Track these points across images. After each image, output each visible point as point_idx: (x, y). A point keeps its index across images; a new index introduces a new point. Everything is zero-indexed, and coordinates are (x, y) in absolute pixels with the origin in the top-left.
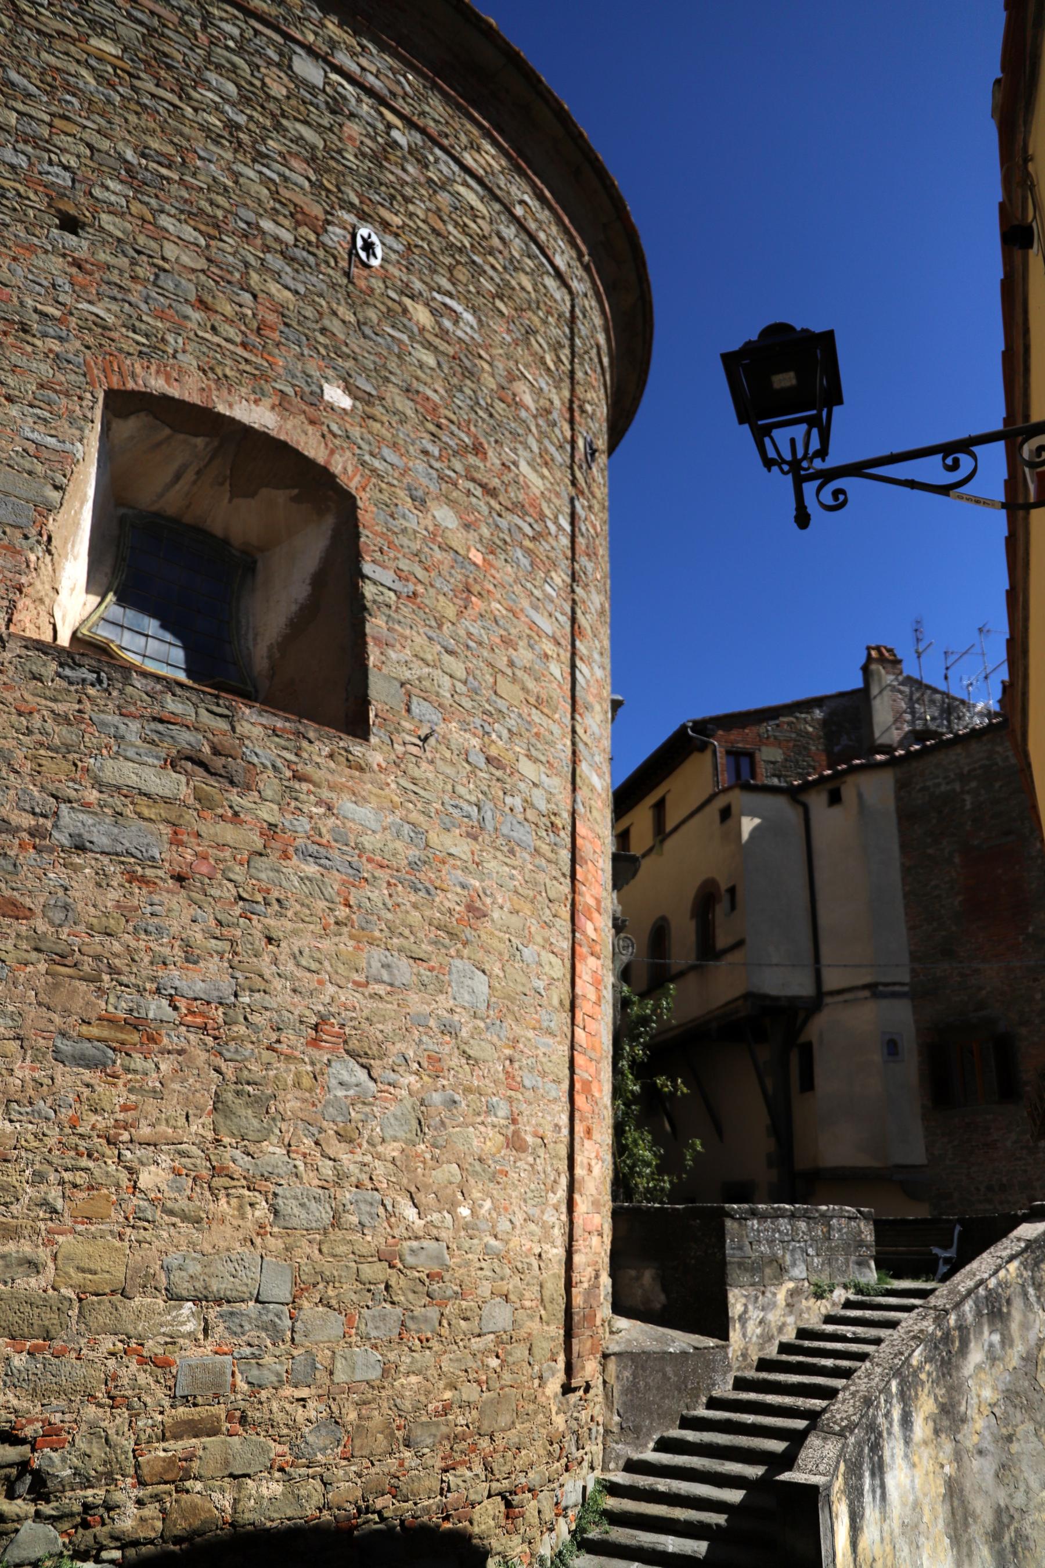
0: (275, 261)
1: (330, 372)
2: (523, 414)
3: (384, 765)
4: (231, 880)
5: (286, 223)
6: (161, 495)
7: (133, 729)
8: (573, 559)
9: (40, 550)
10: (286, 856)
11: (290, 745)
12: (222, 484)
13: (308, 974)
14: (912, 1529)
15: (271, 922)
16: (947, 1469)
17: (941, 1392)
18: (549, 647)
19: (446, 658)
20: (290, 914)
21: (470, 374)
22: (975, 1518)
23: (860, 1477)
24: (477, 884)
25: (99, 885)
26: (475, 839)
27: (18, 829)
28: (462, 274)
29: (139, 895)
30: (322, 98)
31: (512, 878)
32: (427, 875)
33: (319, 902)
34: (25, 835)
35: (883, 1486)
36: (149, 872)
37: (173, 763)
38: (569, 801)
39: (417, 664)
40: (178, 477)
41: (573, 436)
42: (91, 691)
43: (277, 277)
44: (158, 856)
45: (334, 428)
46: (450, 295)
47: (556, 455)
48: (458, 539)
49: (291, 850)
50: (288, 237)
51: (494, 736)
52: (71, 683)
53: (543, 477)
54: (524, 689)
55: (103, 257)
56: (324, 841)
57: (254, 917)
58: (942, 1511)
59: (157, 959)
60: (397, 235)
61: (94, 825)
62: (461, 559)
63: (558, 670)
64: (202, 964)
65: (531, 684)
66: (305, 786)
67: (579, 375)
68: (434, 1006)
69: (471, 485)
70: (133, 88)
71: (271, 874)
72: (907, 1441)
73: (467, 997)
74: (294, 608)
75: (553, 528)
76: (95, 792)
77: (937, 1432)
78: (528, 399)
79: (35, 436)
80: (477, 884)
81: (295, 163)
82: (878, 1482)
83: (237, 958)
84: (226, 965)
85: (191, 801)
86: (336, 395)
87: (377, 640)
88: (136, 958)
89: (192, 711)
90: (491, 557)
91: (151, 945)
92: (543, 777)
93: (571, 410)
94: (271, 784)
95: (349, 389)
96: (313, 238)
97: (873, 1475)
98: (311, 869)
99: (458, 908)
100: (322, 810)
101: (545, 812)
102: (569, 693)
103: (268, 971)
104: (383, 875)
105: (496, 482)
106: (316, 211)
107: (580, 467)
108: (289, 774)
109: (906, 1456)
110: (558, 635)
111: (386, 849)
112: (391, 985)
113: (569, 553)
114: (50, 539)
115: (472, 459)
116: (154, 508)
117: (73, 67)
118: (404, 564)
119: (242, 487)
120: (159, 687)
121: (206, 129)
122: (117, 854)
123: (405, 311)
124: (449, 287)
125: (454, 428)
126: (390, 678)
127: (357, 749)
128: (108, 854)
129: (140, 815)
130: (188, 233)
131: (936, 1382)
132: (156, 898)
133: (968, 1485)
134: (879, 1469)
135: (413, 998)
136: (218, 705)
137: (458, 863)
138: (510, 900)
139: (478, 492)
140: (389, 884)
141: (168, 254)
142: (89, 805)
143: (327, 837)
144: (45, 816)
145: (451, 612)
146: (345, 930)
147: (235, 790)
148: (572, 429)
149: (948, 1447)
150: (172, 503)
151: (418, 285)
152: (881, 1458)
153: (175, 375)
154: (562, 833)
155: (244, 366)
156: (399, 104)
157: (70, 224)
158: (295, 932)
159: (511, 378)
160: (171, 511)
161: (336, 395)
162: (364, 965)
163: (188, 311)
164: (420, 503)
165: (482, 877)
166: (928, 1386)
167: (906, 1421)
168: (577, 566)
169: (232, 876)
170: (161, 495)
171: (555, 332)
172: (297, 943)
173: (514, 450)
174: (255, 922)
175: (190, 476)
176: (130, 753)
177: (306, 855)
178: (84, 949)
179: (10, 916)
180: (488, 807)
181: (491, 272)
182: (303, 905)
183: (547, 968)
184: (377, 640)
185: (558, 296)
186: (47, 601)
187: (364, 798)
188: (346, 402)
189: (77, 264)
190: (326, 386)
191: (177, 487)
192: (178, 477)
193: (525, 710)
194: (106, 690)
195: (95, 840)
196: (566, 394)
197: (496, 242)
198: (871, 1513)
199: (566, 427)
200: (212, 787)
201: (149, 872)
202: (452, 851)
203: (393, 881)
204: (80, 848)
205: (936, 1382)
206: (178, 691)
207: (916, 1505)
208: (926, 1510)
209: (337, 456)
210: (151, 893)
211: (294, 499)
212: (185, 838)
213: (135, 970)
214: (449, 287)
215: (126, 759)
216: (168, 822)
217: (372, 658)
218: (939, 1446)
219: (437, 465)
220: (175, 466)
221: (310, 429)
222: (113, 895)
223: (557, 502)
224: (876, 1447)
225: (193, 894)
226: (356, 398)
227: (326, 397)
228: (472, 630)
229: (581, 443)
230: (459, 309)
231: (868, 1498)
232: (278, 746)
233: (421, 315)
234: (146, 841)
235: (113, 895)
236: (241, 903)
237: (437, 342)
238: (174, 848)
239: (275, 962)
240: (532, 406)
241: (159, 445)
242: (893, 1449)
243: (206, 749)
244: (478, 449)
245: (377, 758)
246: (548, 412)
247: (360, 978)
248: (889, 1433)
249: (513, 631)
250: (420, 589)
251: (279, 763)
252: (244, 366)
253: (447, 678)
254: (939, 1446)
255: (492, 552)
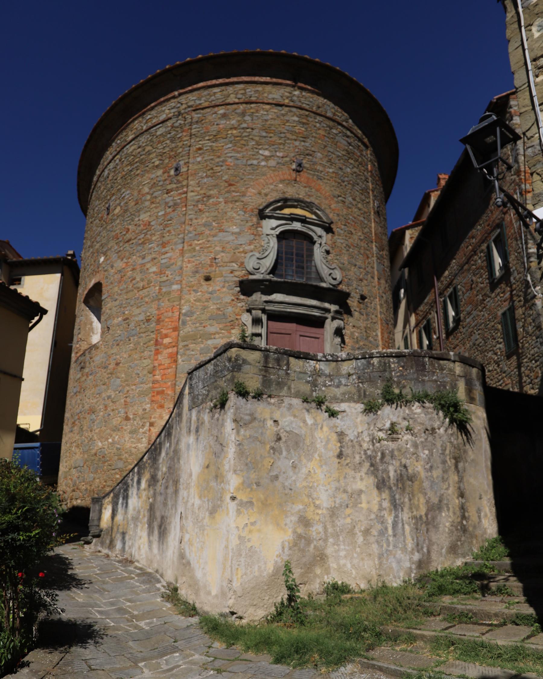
14: (136, 519)
16: (151, 500)
17: (152, 470)
22: (156, 519)
23: (118, 499)
35: (127, 503)
58: (147, 514)
72: (138, 489)
77: (149, 486)
82: (125, 501)
97: (123, 499)
109: (137, 494)
127: (238, 279)
131: (151, 467)
133: (156, 506)
134: (126, 498)
149: (152, 492)
152: (127, 494)
166: (148, 468)
167: (139, 482)
198: (120, 510)
205: (151, 467)
207: (139, 512)
208: (142, 513)
218: (149, 491)
224: (126, 490)
231: (120, 506)
242: (133, 492)
248: (132, 486)
254: (149, 491)
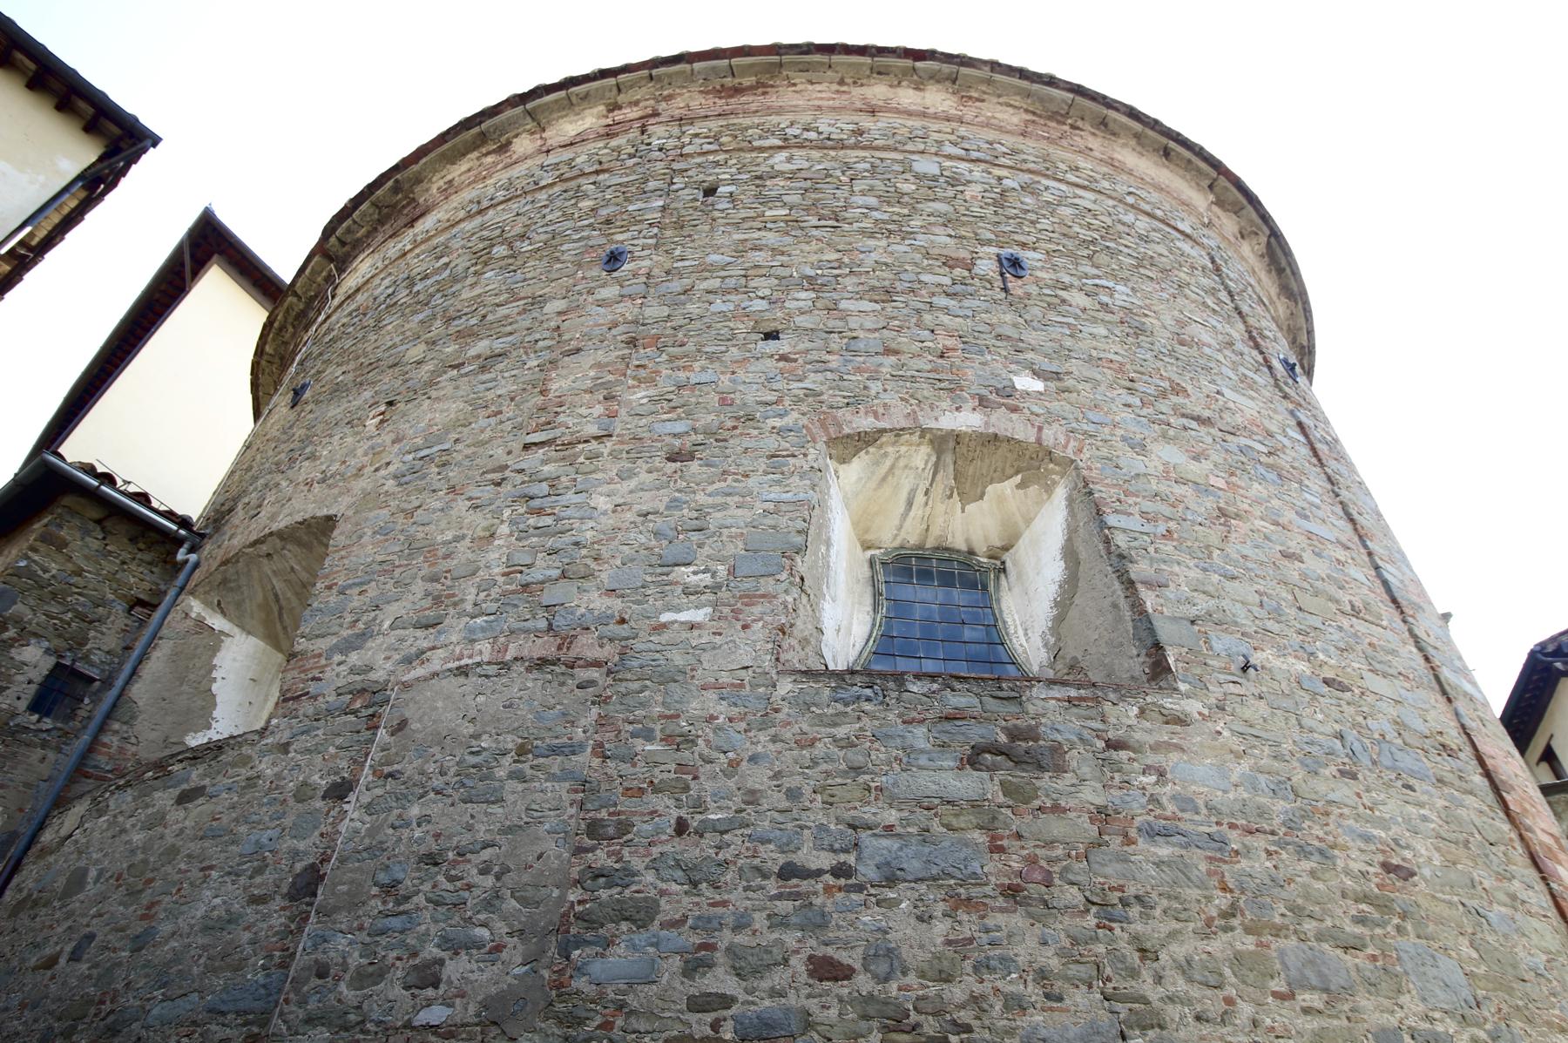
0: (942, 301)
1: (1013, 367)
2: (1206, 350)
3: (1206, 712)
4: (1072, 883)
5: (941, 271)
6: (900, 528)
7: (920, 737)
8: (1322, 465)
9: (795, 592)
10: (1129, 841)
11: (1092, 713)
12: (951, 496)
13: (1209, 992)
15: (1138, 927)
18: (1341, 554)
19: (1228, 584)
20: (1158, 912)
21: (1140, 331)
24: (1383, 835)
25: (920, 919)
26: (1354, 777)
27: (819, 873)
28: (1103, 258)
29: (968, 924)
30: (942, 180)
31: (1425, 819)
32: (1314, 831)
33: (1188, 891)
34: (829, 878)
36: (975, 891)
37: (973, 759)
38: (1450, 715)
39: (1200, 599)
40: (910, 504)
41: (1265, 359)
42: (867, 707)
43: (946, 310)
44: (979, 871)
45: (1036, 409)
46: (1099, 277)
47: (1256, 377)
48: (1195, 469)
49: (1133, 833)
50: (947, 281)
51: (1321, 656)
52: (846, 705)
53: (1253, 398)
54: (1331, 599)
55: (801, 347)
56: (1168, 813)
57: (1114, 925)
59: (1011, 1003)
60: (1034, 249)
61: (901, 849)
62: (1203, 489)
63: (1359, 573)
64: (1068, 1002)
65: (1340, 594)
66: (1123, 755)
67: (1245, 309)
68: (1400, 1014)
69: (1185, 421)
70: (802, 229)
71: (1119, 866)
73: (1441, 995)
74: (1054, 588)
75: (1286, 441)
76: (893, 812)
78: (1206, 337)
79: (772, 496)
80: (1383, 835)
81: (937, 230)
83: (1109, 985)
84: (1099, 996)
85: (1001, 799)
86: (1026, 383)
87: (1148, 584)
88: (985, 1006)
89: (976, 701)
90: (1234, 479)
91: (999, 984)
92: (1403, 692)
93: (1251, 338)
94: (1085, 760)
95: (1037, 374)
96: (966, 273)
98: (1164, 851)
99: (1371, 870)
100: (1153, 778)
101: (1428, 733)
102: (1385, 596)
103: (1154, 993)
104: (1259, 842)
105: (1206, 414)
106: (963, 254)
107: (1286, 384)
108: (1101, 744)
110: (1343, 539)
111: (1247, 810)
112: (1326, 990)
113: (1314, 460)
114: (802, 579)
115: (1174, 399)
116: (897, 543)
117: (756, 235)
118: (1148, 506)
119: (967, 490)
120: (935, 686)
121: (862, 232)
122: (935, 879)
123: (1064, 301)
124: (1095, 271)
125: (1146, 378)
126: (1174, 619)
128: (922, 880)
129: (950, 828)
130: (866, 305)
132: (990, 922)
135: (1365, 1002)
136: (1000, 688)
137: (1346, 811)
138: (1438, 849)
139: (1194, 424)
140: (1269, 853)
141: (852, 325)
142: (889, 828)
143: (1171, 808)
144: (846, 851)
145: (1214, 540)
146: (1235, 922)
147: (1047, 775)
148: (1262, 353)
150: (911, 535)
151: (1067, 279)
153: (881, 411)
154: (1461, 755)
155: (939, 385)
156: (1002, 161)
157: (771, 336)
158: (1173, 935)
159: (1182, 324)
160: (913, 540)
161: (1026, 383)
162: (1278, 966)
163: (880, 359)
164: (1141, 448)
165: (1384, 824)
168: (1329, 471)
169: (1071, 877)
170: (900, 528)
171: (1205, 281)
172: (1179, 950)
173: (1213, 382)
174: (1118, 931)
175: (920, 498)
176: (923, 761)
177: (1153, 834)
178: (921, 1005)
179: (828, 979)
180: (1351, 735)
181: (1126, 250)
182: (1169, 897)
183: (1535, 939)
184: (1148, 584)
185: (1193, 253)
186: (813, 641)
187: (1196, 753)
188: (1038, 385)
189: (783, 358)
190: (1015, 379)
191: (912, 514)
192: (910, 504)
193: (1345, 623)
194: (882, 703)
195: (904, 866)
196: (1241, 327)
197: (1120, 228)
199: (1255, 353)
200: (1021, 776)
201: (975, 891)
202: (1332, 796)
203: (1273, 848)
204: (891, 881)
206: (958, 686)
209: (1045, 431)
210: (983, 917)
211: (1022, 485)
212: (1005, 843)
213: (987, 1022)
214: (1095, 271)
215: (921, 768)
216: (981, 828)
217: (1148, 604)
219: (1145, 412)
220: (904, 495)
221: (1014, 416)
222: (941, 928)
223: (1280, 418)
225: (1031, 909)
226: (1046, 380)
227: (1018, 387)
228: (1245, 552)
229: (1276, 364)
230: (1111, 284)
232: (1079, 717)
233: (1078, 299)
234: (962, 856)
235: (941, 928)
236: (1094, 909)
237: (1101, 315)
238: (996, 856)
239: (1159, 979)
240: (1213, 343)
241: (884, 479)
243: (1003, 738)
244: (1178, 390)
245: (1193, 707)
246: (1231, 344)
247: (1278, 985)
249: (1290, 543)
250: (1172, 525)
251: (1085, 733)
252: (939, 385)
253: (1238, 605)
255: (1232, 474)
